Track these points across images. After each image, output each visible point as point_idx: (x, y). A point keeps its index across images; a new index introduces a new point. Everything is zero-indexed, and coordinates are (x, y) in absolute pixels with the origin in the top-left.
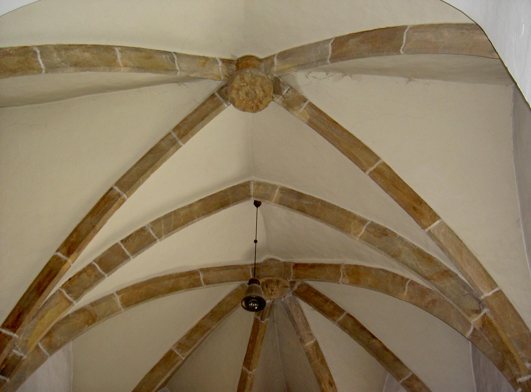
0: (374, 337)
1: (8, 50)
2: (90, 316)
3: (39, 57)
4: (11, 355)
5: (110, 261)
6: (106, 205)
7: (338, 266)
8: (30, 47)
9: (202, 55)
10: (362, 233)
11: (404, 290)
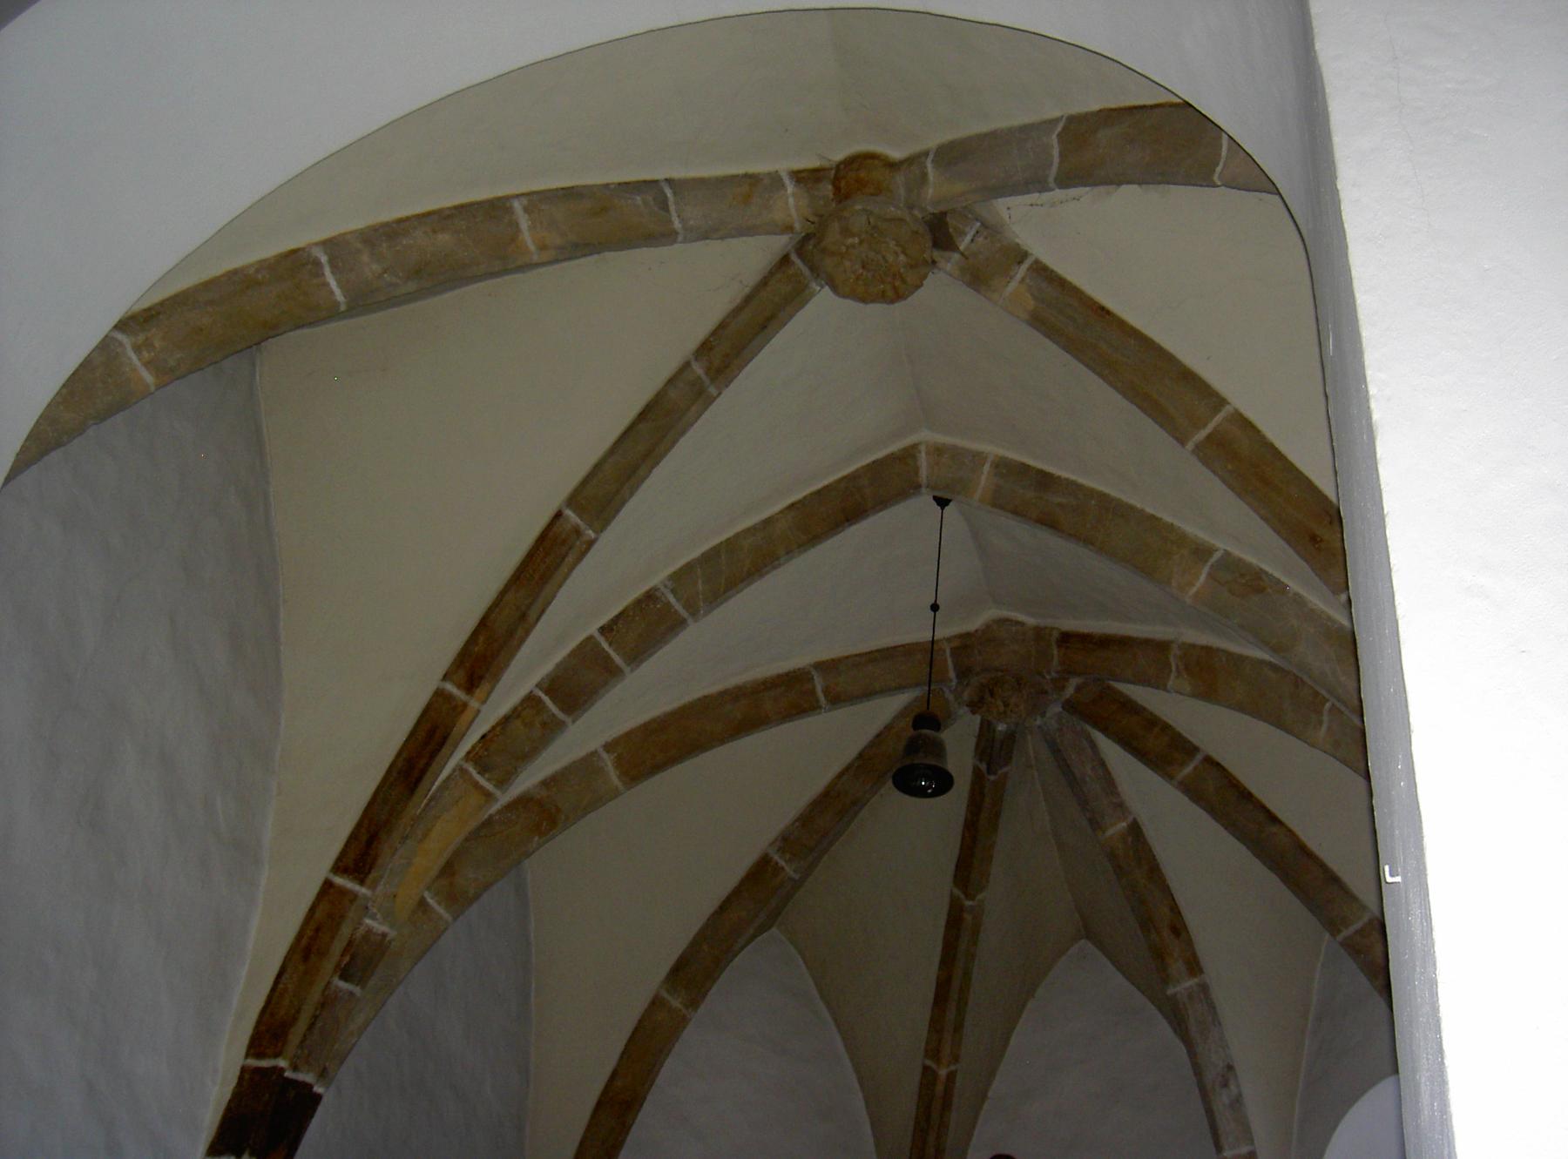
0: (1274, 819)
1: (252, 271)
2: (544, 815)
3: (327, 271)
4: (361, 931)
5: (573, 687)
6: (549, 557)
7: (1162, 647)
8: (302, 249)
9: (741, 171)
10: (1198, 585)
11: (1320, 723)
